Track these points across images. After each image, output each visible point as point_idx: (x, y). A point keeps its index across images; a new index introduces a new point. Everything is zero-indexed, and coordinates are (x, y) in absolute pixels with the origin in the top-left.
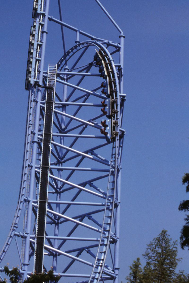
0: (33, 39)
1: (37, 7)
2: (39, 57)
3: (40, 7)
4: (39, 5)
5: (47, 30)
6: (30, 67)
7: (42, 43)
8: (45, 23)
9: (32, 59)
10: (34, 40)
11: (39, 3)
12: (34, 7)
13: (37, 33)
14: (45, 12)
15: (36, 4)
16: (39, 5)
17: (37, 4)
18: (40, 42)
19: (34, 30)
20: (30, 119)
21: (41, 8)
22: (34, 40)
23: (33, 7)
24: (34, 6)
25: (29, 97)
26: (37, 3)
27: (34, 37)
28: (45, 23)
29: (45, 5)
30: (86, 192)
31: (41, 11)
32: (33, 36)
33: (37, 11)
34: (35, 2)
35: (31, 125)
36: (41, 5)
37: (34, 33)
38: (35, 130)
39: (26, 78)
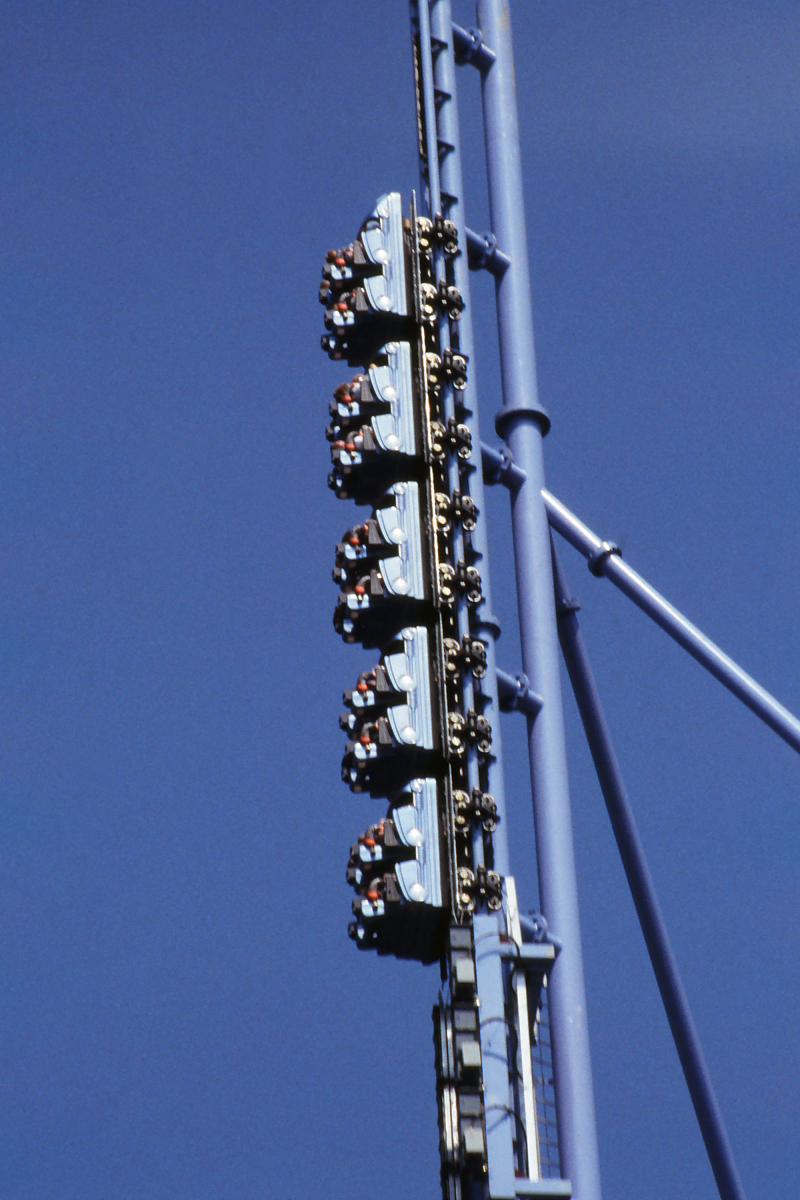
0: (465, 1111)
1: (474, 1143)
2: (547, 1171)
3: (507, 1130)
4: (500, 1114)
5: (541, 398)
6: (455, 956)
7: (546, 952)
8: (574, 1186)
9: (469, 963)
10: (476, 1119)
11: (491, 1099)
12: (449, 1146)
13: (503, 1052)
14: (563, 1175)
15: (461, 1117)
16: (491, 1117)
17: (476, 1112)
18: (528, 936)
19: (466, 1032)
20: (436, 36)
21: (519, 1146)
22: (476, 1119)
23: (442, 1143)
24: (451, 1140)
25: (425, 175)
26: (471, 1105)
27: (476, 1100)
28: (574, 1186)
29: (554, 1152)
30: (751, 714)
31: (522, 1171)
32: (469, 1081)
33: (484, 1178)
34: (450, 1097)
35: (495, 631)
36: (516, 1113)
37: (471, 1054)
38: (513, 451)
39: (434, 1072)
